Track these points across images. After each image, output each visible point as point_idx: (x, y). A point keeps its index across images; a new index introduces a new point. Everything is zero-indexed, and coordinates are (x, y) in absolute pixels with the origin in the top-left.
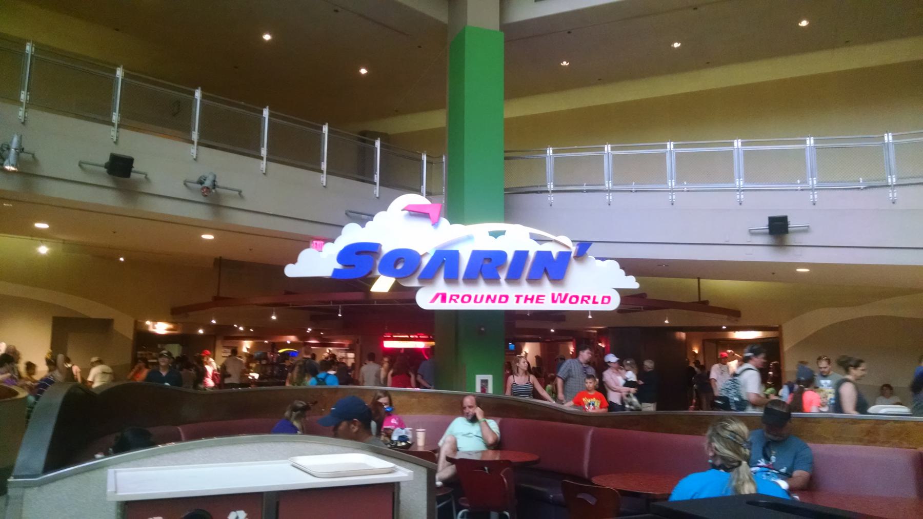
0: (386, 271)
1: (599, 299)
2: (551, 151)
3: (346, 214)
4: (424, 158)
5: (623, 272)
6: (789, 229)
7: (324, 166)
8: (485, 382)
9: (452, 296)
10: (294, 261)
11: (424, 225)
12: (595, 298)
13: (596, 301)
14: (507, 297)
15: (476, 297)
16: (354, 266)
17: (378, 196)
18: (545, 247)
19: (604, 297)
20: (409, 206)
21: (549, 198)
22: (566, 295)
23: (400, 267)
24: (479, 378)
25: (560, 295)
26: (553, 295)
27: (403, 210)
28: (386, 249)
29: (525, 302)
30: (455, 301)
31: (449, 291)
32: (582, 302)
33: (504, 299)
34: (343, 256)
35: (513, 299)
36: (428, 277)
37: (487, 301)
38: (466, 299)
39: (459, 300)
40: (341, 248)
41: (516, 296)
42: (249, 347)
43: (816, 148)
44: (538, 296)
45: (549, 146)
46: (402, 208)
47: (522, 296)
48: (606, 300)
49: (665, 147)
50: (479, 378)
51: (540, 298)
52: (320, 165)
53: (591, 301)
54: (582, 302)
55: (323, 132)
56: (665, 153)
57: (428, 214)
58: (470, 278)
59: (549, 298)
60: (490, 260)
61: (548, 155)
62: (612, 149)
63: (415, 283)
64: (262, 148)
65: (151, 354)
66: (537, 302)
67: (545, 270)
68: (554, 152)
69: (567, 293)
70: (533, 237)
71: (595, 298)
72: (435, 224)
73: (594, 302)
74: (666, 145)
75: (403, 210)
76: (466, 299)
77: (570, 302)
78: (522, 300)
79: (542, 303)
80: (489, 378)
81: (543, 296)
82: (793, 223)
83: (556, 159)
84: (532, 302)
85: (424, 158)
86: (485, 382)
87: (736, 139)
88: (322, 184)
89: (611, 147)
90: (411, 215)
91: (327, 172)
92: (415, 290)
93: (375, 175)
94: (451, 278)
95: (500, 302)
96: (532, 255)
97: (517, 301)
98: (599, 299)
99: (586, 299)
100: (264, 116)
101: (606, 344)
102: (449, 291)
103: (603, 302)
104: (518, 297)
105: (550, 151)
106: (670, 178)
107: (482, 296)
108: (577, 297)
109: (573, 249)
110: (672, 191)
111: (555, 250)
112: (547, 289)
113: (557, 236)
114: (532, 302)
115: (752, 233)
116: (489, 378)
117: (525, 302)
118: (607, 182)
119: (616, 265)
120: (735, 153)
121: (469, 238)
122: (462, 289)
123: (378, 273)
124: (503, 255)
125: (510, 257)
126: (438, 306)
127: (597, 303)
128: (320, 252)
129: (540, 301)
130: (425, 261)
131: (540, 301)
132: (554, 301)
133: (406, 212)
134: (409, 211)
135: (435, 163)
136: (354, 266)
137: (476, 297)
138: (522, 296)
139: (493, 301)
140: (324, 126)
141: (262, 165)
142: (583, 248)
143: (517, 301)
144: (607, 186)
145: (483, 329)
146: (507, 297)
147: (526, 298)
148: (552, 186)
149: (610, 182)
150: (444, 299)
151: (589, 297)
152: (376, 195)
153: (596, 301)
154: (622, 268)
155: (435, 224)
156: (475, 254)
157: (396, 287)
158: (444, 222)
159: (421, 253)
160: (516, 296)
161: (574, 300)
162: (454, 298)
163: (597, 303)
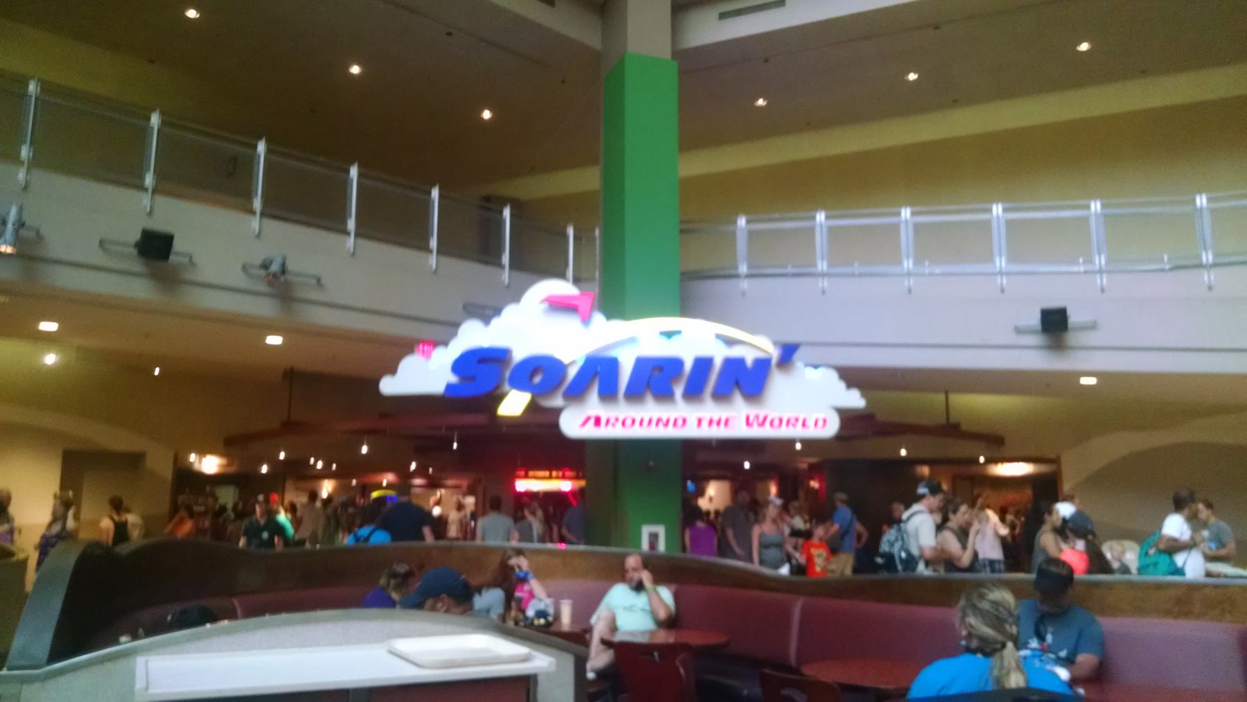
7: (434, 243)
10: (392, 370)
11: (571, 323)
18: (736, 352)
23: (537, 379)
24: (646, 530)
25: (757, 417)
28: (518, 355)
31: (604, 412)
35: (692, 422)
36: (576, 392)
39: (619, 424)
50: (646, 530)
67: (737, 384)
72: (586, 320)
78: (705, 424)
80: (661, 530)
83: (1009, 223)
85: (571, 231)
92: (557, 412)
94: (608, 394)
96: (718, 363)
101: (821, 481)
105: (742, 221)
110: (909, 274)
111: (750, 356)
115: (1019, 331)
116: (661, 530)
119: (833, 376)
120: (902, 227)
123: (506, 387)
124: (676, 364)
126: (590, 432)
130: (572, 372)
139: (762, 424)
142: (788, 353)
145: (651, 463)
147: (711, 422)
155: (586, 320)
156: (641, 363)
157: (533, 407)
158: (598, 318)
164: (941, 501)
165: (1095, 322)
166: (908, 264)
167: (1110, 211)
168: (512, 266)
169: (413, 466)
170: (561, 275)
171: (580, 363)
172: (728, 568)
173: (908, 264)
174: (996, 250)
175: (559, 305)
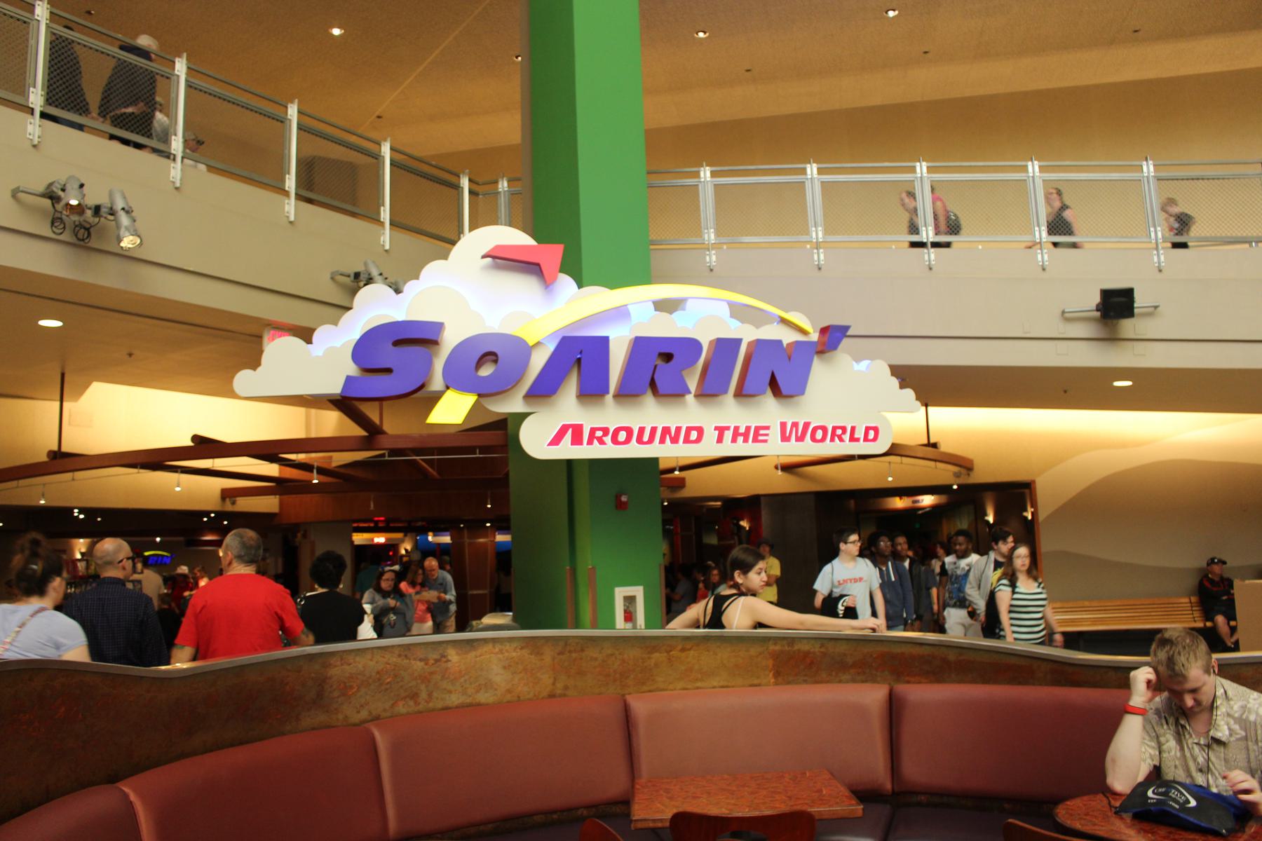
0: (455, 380)
1: (860, 434)
2: (708, 174)
3: (332, 278)
4: (465, 183)
5: (895, 382)
6: (1136, 310)
8: (630, 600)
9: (593, 430)
11: (522, 287)
12: (853, 429)
13: (856, 436)
14: (700, 431)
15: (642, 430)
16: (389, 371)
17: (387, 247)
18: (772, 332)
19: (867, 429)
20: (497, 247)
21: (708, 258)
22: (807, 425)
24: (620, 593)
25: (795, 425)
26: (783, 425)
27: (484, 257)
28: (451, 339)
29: (734, 440)
30: (601, 442)
31: (589, 418)
32: (832, 440)
33: (694, 435)
34: (363, 349)
35: (710, 435)
36: (544, 389)
37: (662, 441)
38: (622, 436)
39: (608, 439)
40: (356, 335)
41: (716, 428)
42: (83, 550)
43: (1158, 180)
44: (757, 429)
45: (704, 164)
46: (483, 253)
47: (728, 428)
48: (871, 435)
49: (913, 170)
50: (620, 593)
51: (762, 432)
52: (283, 181)
53: (847, 437)
54: (832, 440)
55: (289, 117)
56: (914, 181)
57: (538, 265)
58: (627, 393)
59: (775, 433)
60: (668, 357)
61: (703, 180)
62: (820, 171)
63: (513, 404)
64: (173, 137)
65: (904, 604)
66: (755, 440)
68: (713, 174)
69: (807, 420)
70: (738, 311)
71: (853, 429)
73: (853, 439)
74: (915, 167)
75: (484, 257)
76: (622, 436)
77: (813, 439)
78: (728, 435)
79: (765, 441)
80: (638, 592)
81: (767, 428)
82: (1140, 301)
83: (717, 187)
84: (746, 441)
85: (465, 183)
86: (630, 600)
87: (810, 163)
88: (288, 217)
89: (818, 169)
90: (497, 267)
91: (296, 194)
93: (382, 208)
94: (592, 391)
95: (687, 441)
97: (720, 440)
98: (860, 434)
99: (599, 434)
100: (176, 72)
102: (589, 418)
103: (866, 439)
104: (721, 430)
106: (923, 224)
107: (654, 430)
108: (824, 429)
109: (814, 337)
110: (817, 246)
112: (769, 412)
113: (787, 311)
114: (746, 441)
115: (1066, 317)
116: (638, 592)
117: (734, 440)
118: (814, 229)
119: (888, 371)
120: (808, 185)
121: (620, 313)
122: (610, 415)
124: (692, 345)
125: (743, 349)
126: (567, 451)
127: (858, 440)
128: (308, 343)
129: (761, 438)
130: (538, 361)
131: (761, 438)
132: (785, 438)
133: (489, 260)
134: (494, 257)
135: (484, 195)
136: (389, 371)
137: (642, 430)
138: (728, 428)
140: (289, 106)
141: (172, 170)
142: (832, 337)
143: (720, 440)
144: (814, 236)
145: (624, 499)
146: (700, 431)
147: (736, 433)
148: (712, 236)
149: (820, 228)
150: (577, 440)
151: (844, 429)
152: (383, 246)
153: (856, 436)
154: (893, 374)
156: (640, 345)
158: (566, 283)
159: (531, 344)
160: (716, 428)
161: (819, 434)
162: (839, 432)
163: (858, 440)
164: (390, 586)
165: (311, 343)
166: (818, 234)
167: (1163, 174)
168: (393, 224)
169: (205, 519)
170: (495, 222)
171: (551, 347)
172: (1257, 583)
173: (818, 234)
174: (811, 222)
175: (502, 259)
